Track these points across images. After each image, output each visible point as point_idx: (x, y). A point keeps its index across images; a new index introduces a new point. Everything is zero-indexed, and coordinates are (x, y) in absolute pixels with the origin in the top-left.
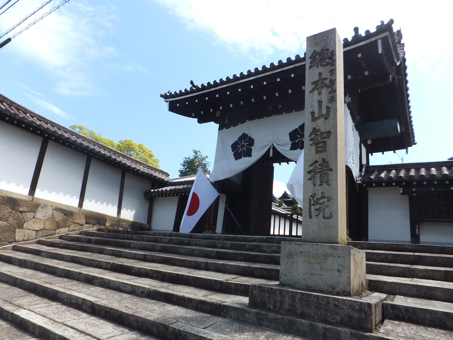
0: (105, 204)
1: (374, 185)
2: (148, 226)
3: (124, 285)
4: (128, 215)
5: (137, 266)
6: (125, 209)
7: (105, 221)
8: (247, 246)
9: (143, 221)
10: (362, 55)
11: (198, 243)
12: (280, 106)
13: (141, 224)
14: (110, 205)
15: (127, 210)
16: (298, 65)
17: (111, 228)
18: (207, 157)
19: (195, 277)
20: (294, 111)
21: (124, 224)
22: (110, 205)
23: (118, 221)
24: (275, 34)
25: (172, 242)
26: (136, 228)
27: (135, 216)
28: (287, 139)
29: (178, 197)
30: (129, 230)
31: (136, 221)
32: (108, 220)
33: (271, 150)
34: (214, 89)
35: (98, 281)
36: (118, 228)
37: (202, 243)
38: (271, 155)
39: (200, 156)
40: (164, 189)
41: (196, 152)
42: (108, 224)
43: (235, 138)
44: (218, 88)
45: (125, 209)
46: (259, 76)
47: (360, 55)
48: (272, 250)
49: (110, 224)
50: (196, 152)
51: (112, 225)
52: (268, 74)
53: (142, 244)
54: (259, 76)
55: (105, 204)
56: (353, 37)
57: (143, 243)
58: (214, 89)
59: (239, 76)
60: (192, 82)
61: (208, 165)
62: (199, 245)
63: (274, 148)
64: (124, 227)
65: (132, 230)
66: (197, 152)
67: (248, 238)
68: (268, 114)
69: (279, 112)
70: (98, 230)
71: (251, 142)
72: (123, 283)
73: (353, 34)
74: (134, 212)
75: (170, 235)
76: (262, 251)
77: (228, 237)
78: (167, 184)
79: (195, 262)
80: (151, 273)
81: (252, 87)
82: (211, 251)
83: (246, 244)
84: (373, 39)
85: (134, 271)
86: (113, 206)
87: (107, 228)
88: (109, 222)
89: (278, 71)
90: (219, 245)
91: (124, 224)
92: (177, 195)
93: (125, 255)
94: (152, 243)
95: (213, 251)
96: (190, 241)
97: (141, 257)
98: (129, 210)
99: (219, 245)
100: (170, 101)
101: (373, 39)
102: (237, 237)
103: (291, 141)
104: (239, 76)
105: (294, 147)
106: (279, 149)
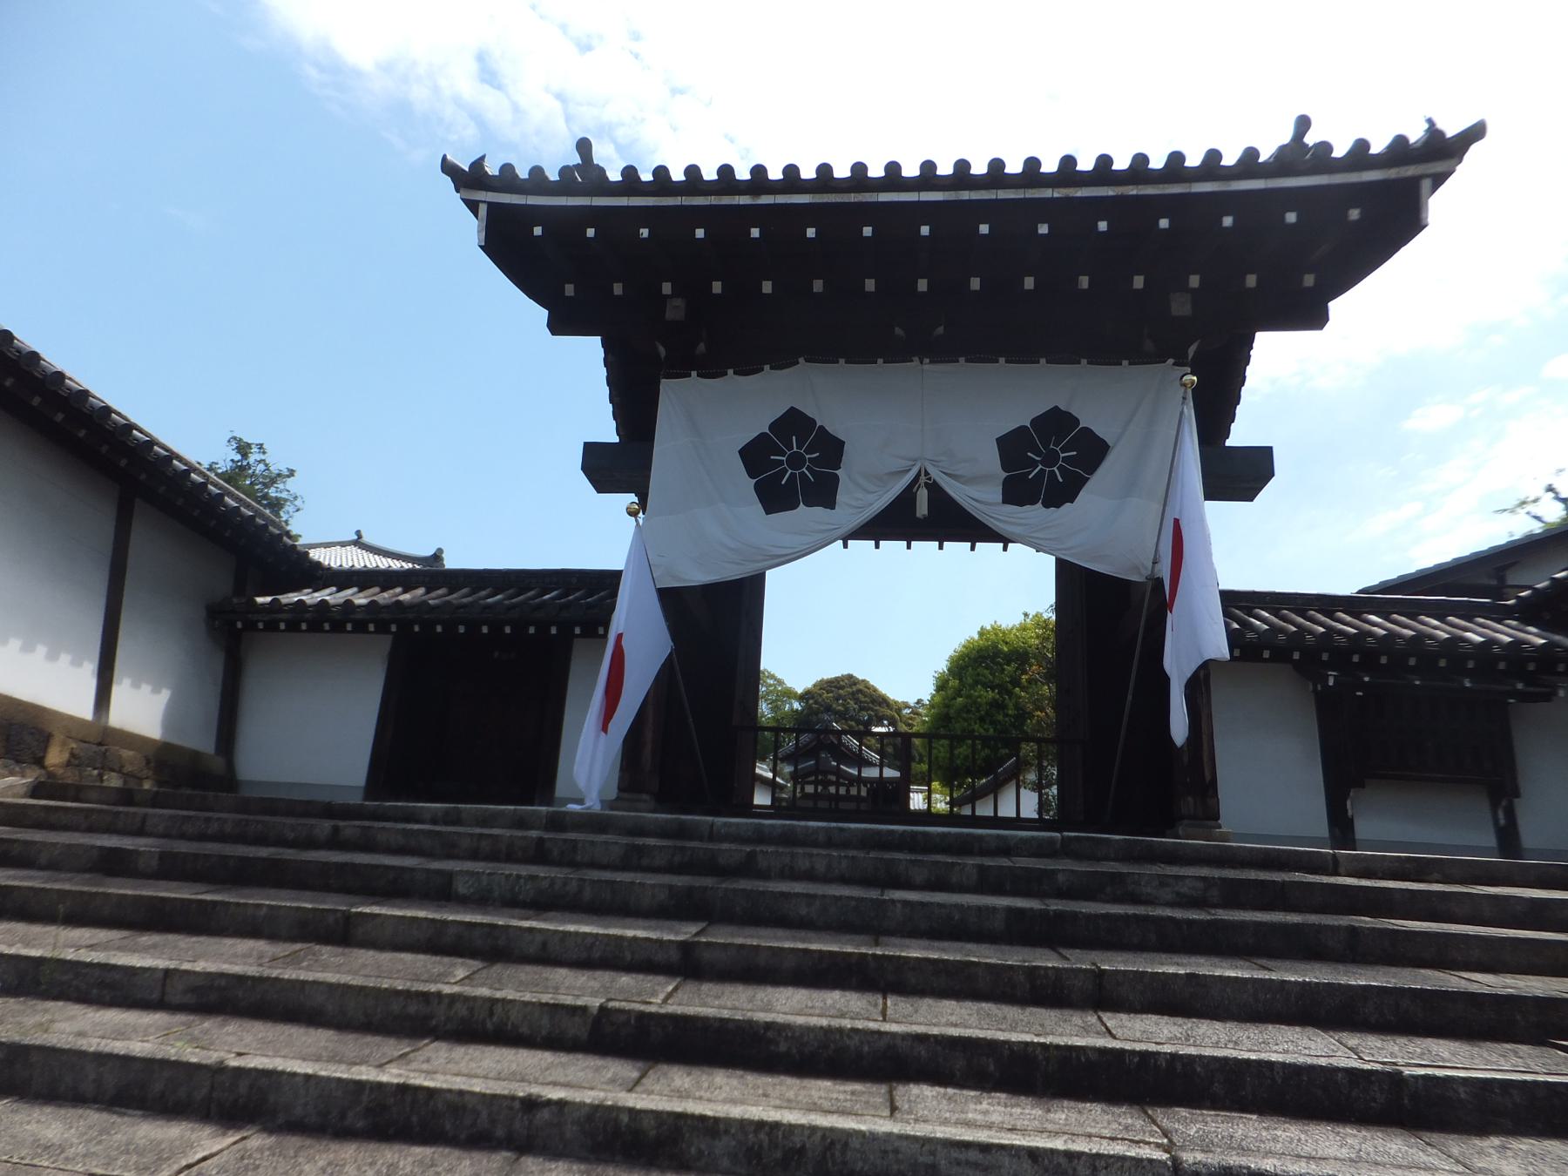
0: (41, 650)
1: (1266, 654)
2: (218, 764)
3: (973, 1155)
4: (141, 710)
5: (200, 966)
6: (127, 682)
7: (46, 739)
8: (1061, 878)
9: (202, 741)
10: (1235, 221)
11: (803, 864)
12: (940, 330)
13: (195, 755)
14: (65, 659)
15: (136, 685)
16: (1132, 191)
17: (70, 777)
18: (292, 473)
19: (1226, 1060)
20: (1002, 360)
21: (127, 754)
22: (65, 659)
23: (100, 742)
24: (489, 75)
25: (645, 862)
26: (187, 778)
27: (172, 717)
28: (991, 461)
29: (390, 637)
30: (147, 786)
31: (169, 740)
32: (58, 737)
33: (923, 496)
34: (744, 200)
35: (722, 1145)
36: (100, 776)
37: (820, 866)
38: (922, 509)
39: (261, 467)
40: (293, 597)
41: (243, 448)
42: (55, 757)
43: (760, 425)
44: (766, 200)
45: (127, 682)
46: (965, 195)
47: (1291, 217)
48: (1178, 894)
49: (66, 756)
50: (243, 448)
51: (74, 761)
52: (1003, 194)
53: (533, 878)
54: (965, 195)
55: (41, 650)
56: (1282, 149)
57: (541, 871)
58: (744, 200)
59: (646, 176)
60: (584, 146)
61: (289, 508)
62: (810, 876)
63: (935, 489)
64: (128, 768)
65: (160, 783)
66: (249, 445)
67: (981, 837)
68: (897, 353)
69: (942, 352)
70: (36, 791)
71: (832, 449)
72: (967, 1145)
73: (1286, 136)
74: (165, 696)
75: (347, 812)
76: (1135, 900)
77: (879, 832)
78: (320, 576)
79: (1033, 971)
80: (922, 1051)
81: (867, 231)
82: (980, 909)
83: (1054, 872)
84: (1410, 171)
85: (783, 1047)
86: (76, 663)
87: (51, 775)
88: (64, 744)
89: (1048, 193)
90: (919, 876)
91: (127, 754)
92: (382, 628)
93: (532, 950)
94: (607, 875)
95: (994, 910)
96: (751, 856)
97: (660, 957)
98: (146, 688)
99: (919, 876)
100: (492, 206)
101: (1410, 171)
102: (925, 834)
103: (1004, 469)
104: (646, 176)
105: (1017, 492)
106: (958, 492)
